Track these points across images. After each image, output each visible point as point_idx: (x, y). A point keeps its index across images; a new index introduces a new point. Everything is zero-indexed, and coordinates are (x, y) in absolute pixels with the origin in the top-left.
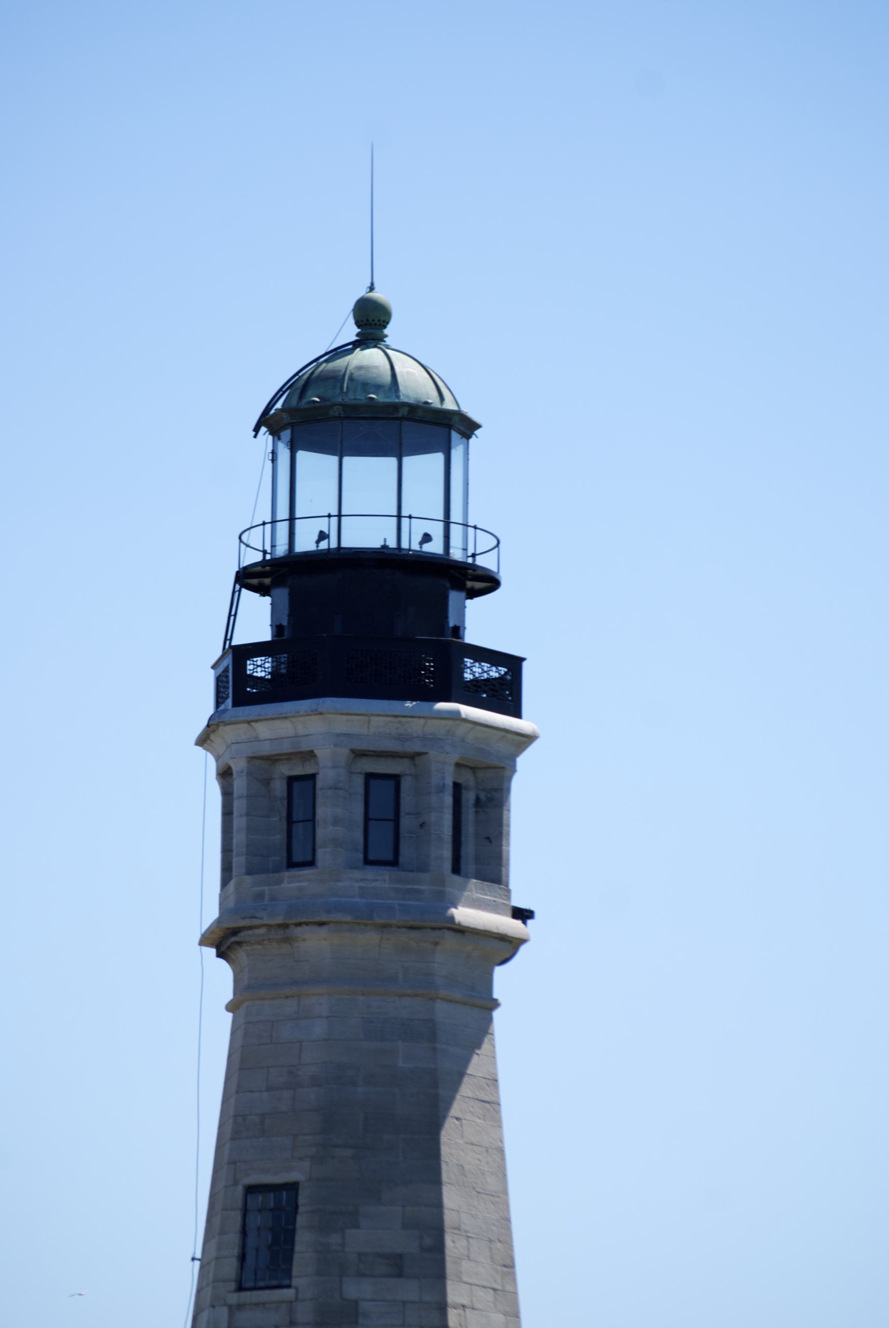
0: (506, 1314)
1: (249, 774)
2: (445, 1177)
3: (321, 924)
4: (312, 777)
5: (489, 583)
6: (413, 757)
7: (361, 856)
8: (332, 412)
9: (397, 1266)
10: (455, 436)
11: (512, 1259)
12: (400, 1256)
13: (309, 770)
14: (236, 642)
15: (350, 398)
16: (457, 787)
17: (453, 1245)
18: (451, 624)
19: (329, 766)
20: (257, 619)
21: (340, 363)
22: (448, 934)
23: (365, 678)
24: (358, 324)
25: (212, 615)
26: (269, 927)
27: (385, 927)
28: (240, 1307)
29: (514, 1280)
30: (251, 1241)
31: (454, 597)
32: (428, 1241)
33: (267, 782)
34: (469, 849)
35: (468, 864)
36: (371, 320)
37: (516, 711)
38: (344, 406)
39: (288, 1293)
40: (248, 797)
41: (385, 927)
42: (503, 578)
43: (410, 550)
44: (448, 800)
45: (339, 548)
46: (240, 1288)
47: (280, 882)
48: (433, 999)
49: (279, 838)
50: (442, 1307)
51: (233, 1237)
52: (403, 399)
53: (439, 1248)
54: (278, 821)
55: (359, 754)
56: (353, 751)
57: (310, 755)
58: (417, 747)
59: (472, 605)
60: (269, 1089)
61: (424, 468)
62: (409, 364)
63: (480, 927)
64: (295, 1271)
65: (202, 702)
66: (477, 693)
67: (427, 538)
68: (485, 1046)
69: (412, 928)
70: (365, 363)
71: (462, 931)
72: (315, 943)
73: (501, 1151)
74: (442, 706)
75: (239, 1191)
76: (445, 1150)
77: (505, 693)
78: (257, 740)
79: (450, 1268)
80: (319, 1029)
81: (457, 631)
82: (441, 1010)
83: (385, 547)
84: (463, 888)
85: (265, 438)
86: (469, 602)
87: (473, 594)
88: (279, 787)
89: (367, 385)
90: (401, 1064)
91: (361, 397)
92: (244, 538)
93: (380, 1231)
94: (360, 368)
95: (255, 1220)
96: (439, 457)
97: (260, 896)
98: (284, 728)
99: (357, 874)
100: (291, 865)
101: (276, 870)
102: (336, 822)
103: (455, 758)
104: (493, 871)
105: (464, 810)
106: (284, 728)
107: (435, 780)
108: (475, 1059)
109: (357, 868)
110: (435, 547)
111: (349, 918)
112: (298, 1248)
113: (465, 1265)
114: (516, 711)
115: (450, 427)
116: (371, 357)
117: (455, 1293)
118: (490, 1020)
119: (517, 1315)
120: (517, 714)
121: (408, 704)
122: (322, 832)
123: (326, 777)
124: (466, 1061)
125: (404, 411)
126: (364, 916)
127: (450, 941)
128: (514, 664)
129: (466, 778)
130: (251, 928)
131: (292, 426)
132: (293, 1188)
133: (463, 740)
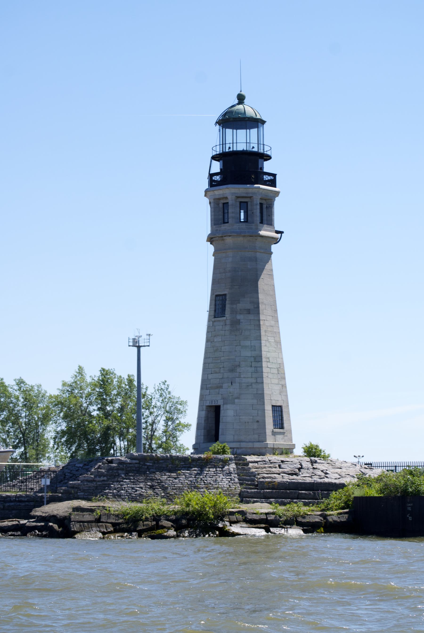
0: (275, 321)
1: (214, 203)
2: (259, 292)
3: (230, 236)
4: (228, 203)
5: (268, 158)
6: (250, 197)
8: (232, 120)
9: (249, 312)
10: (259, 124)
11: (277, 309)
12: (249, 309)
13: (227, 201)
14: (210, 173)
15: (235, 116)
16: (261, 204)
17: (261, 307)
18: (260, 167)
19: (231, 200)
20: (217, 167)
21: (233, 109)
22: (259, 237)
23: (241, 176)
24: (238, 99)
25: (203, 167)
26: (219, 237)
27: (244, 236)
28: (215, 321)
29: (277, 314)
30: (217, 307)
31: (260, 161)
32: (256, 306)
33: (218, 204)
34: (265, 218)
35: (265, 221)
36: (241, 99)
37: (275, 186)
38: (233, 118)
39: (225, 318)
40: (214, 208)
41: (244, 236)
42: (272, 156)
43: (247, 150)
44: (258, 207)
45: (233, 150)
46: (215, 317)
47: (221, 227)
48: (256, 252)
49: (221, 217)
50: (259, 320)
51: (213, 306)
52: (247, 116)
53: (258, 307)
54: (221, 213)
55: (238, 197)
56: (236, 197)
57: (226, 198)
58: (251, 195)
59: (266, 163)
60: (220, 273)
61: (254, 131)
62: (249, 109)
63: (267, 235)
64: (226, 313)
66: (265, 183)
67: (253, 147)
68: (270, 262)
69: (250, 236)
70: (238, 108)
71: (262, 237)
72: (229, 240)
73: (274, 286)
74: (256, 185)
75: (214, 296)
76: (259, 286)
77: (273, 183)
78: (215, 195)
79: (261, 312)
80: (230, 260)
81: (262, 168)
82: (258, 255)
83: (243, 150)
84: (263, 227)
85: (218, 126)
86: (264, 162)
87: (266, 160)
88: (221, 205)
89: (238, 113)
90: (249, 267)
91: (237, 116)
92: (214, 149)
93: (244, 304)
94: (237, 109)
95: (218, 302)
96: (257, 129)
97: (217, 230)
98: (221, 192)
99: (238, 224)
100: (224, 223)
101: (221, 224)
102: (232, 213)
103: (260, 197)
104: (270, 223)
105: (263, 209)
106: (221, 192)
107: (255, 202)
108: (267, 265)
109: (238, 223)
110: (255, 149)
111: (235, 234)
112: (226, 308)
113: (265, 311)
114: (275, 186)
115: (258, 122)
116: (241, 107)
117: (262, 317)
118: (271, 257)
119: (278, 322)
120: (275, 187)
121: (248, 185)
122: (230, 215)
123: (230, 203)
124: (265, 266)
125: (247, 119)
126: (239, 234)
127: (259, 238)
128: (274, 175)
129: (263, 202)
130: (215, 237)
131: (222, 123)
132: (225, 295)
133: (261, 193)
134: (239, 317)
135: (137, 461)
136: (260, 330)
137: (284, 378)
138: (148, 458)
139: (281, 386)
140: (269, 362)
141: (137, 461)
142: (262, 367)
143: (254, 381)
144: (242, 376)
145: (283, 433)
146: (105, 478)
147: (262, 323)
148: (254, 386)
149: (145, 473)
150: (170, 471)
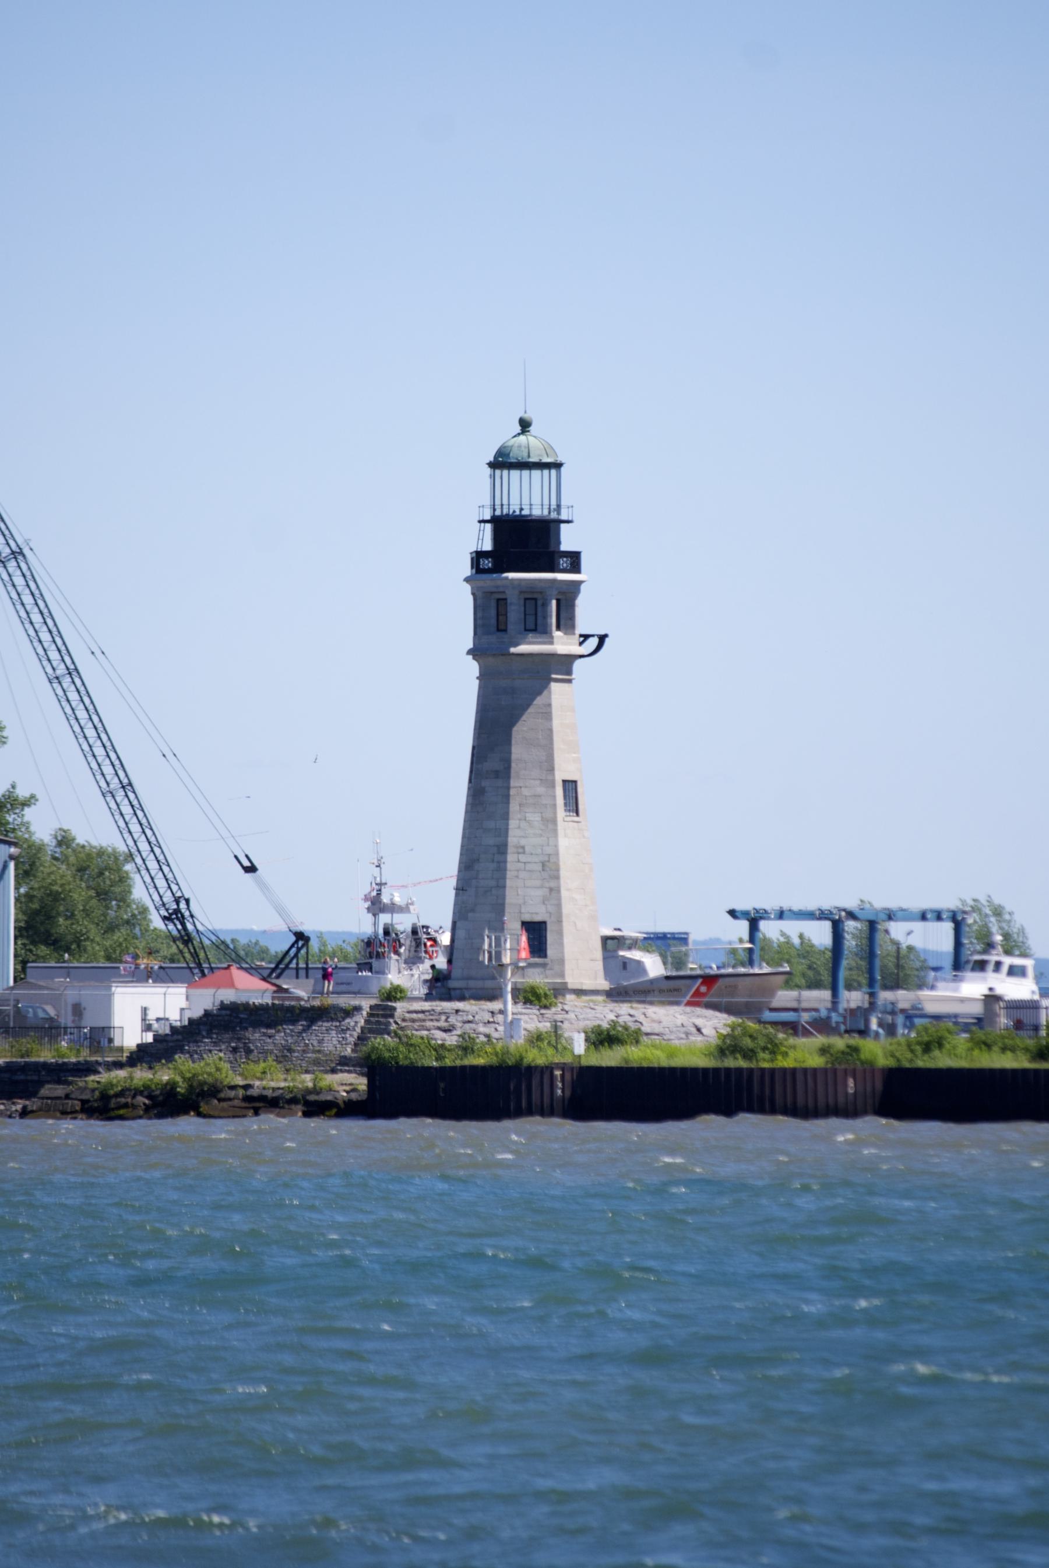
4: (506, 599)
6: (541, 593)
7: (522, 627)
9: (497, 774)
23: (523, 560)
36: (525, 425)
46: (564, 781)
50: (508, 788)
55: (521, 592)
62: (532, 445)
65: (468, 571)
68: (545, 693)
71: (513, 654)
117: (513, 783)
134: (485, 783)
135: (228, 1012)
136: (508, 803)
137: (557, 878)
138: (241, 1008)
139: (547, 891)
140: (524, 853)
141: (228, 1012)
142: (505, 862)
143: (493, 883)
144: (481, 876)
145: (544, 966)
146: (180, 1037)
147: (512, 792)
148: (494, 892)
149: (234, 1030)
150: (269, 1026)
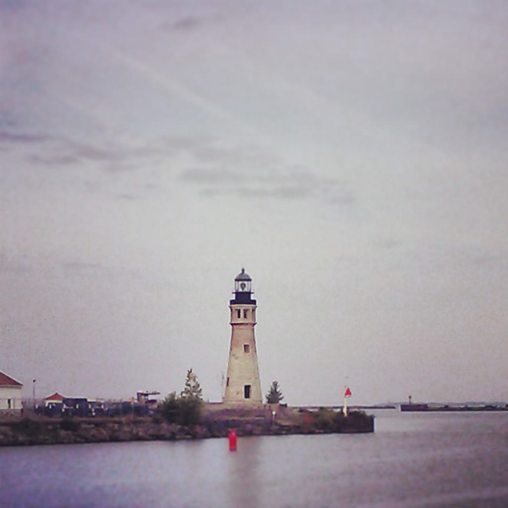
23: (243, 298)
